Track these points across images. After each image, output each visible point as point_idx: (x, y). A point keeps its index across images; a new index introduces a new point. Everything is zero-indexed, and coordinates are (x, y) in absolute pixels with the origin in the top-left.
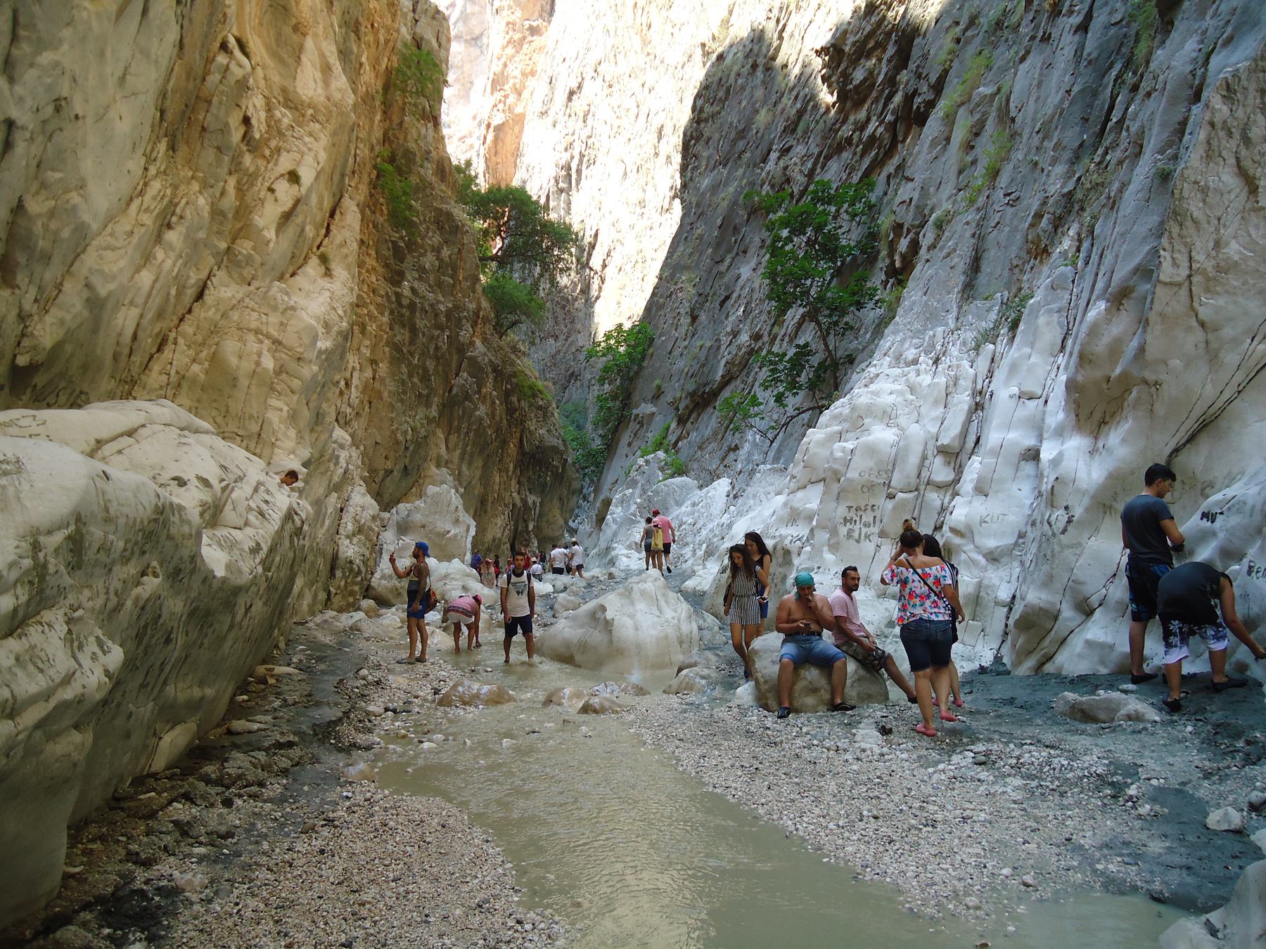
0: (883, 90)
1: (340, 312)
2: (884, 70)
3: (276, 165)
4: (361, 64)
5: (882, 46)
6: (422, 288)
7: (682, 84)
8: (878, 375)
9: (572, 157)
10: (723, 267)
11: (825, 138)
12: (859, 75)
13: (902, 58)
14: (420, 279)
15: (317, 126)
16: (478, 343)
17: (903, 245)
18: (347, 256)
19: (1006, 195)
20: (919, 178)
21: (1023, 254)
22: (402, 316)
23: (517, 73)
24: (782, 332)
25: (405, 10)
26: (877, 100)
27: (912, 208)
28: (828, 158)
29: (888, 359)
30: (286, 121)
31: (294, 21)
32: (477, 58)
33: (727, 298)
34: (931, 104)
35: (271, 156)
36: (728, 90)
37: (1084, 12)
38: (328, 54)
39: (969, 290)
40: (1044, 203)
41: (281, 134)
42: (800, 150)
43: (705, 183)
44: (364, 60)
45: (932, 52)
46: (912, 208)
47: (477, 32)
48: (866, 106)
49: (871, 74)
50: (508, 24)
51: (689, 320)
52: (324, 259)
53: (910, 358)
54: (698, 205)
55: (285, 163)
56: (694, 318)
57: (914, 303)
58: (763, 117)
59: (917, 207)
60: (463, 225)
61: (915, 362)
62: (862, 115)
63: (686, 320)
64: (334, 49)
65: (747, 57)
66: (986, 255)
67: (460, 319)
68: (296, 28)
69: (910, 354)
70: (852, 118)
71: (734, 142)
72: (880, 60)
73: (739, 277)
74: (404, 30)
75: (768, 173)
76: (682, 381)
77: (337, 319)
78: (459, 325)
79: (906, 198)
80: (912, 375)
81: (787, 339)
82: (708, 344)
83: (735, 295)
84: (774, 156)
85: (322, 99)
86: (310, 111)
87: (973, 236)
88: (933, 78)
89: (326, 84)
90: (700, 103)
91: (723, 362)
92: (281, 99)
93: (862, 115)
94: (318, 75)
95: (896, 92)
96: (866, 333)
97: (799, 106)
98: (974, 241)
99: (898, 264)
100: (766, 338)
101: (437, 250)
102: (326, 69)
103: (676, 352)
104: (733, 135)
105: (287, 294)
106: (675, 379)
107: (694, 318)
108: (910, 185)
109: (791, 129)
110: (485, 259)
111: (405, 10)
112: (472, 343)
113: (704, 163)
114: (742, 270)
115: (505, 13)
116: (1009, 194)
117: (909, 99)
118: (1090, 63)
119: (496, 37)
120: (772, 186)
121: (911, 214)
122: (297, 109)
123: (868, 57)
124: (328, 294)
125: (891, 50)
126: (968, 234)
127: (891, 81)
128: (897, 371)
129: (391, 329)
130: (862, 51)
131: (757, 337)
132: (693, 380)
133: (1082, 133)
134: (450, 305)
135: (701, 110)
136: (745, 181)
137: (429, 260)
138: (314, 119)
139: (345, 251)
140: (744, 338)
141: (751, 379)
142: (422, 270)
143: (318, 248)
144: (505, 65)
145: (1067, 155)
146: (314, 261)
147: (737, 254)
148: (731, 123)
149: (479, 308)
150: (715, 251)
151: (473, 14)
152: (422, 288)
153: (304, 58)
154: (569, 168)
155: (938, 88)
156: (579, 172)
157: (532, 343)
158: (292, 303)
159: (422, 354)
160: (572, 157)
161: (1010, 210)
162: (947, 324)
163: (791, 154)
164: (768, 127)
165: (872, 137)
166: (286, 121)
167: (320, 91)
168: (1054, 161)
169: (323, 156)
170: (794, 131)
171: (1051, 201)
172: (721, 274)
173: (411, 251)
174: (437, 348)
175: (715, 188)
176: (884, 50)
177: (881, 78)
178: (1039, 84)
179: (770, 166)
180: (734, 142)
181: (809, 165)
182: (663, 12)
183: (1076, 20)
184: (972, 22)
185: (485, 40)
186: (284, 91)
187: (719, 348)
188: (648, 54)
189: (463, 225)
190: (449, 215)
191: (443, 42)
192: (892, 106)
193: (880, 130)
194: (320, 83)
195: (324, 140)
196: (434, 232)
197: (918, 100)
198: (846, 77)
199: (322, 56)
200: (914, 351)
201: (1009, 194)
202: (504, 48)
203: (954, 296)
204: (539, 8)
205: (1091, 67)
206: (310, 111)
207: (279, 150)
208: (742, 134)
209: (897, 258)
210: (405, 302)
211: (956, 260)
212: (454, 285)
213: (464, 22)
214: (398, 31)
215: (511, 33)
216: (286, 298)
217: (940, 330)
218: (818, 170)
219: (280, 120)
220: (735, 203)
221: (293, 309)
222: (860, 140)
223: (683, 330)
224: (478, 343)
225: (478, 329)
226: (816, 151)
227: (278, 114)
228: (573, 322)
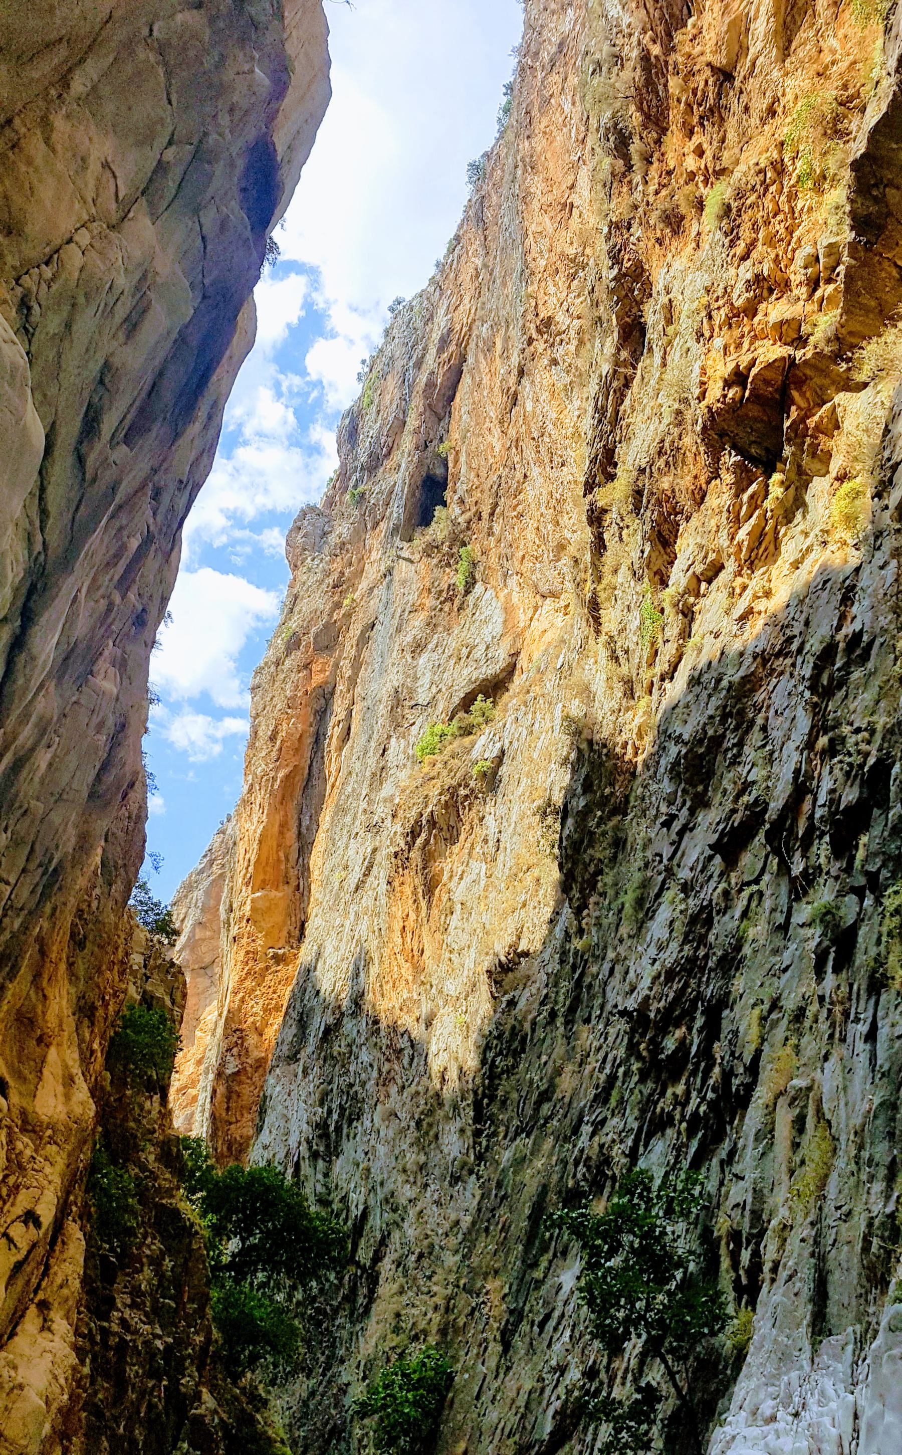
0: (697, 1065)
1: (62, 1381)
2: (696, 1041)
3: (13, 1205)
4: (93, 1052)
5: (689, 1014)
6: (134, 1318)
7: (467, 1018)
8: (734, 1438)
9: (330, 1112)
10: (538, 1274)
11: (643, 1111)
12: (670, 1044)
13: (712, 1031)
14: (133, 1306)
15: (54, 1148)
16: (206, 1396)
17: (745, 1256)
18: (67, 1300)
19: (838, 1208)
20: (751, 1176)
21: (864, 1282)
22: (108, 1361)
23: (257, 1009)
24: (625, 1365)
25: (135, 967)
26: (694, 1073)
27: (747, 1213)
28: (650, 1136)
29: (743, 1413)
30: (28, 1152)
31: (39, 1032)
32: (206, 989)
33: (548, 1317)
34: (750, 1088)
35: (9, 1196)
36: (524, 1039)
37: (869, 1021)
38: (70, 1063)
39: (820, 1326)
40: (870, 1225)
41: (21, 1167)
42: (615, 1122)
43: (506, 1156)
44: (96, 1046)
45: (741, 1029)
46: (747, 1213)
47: (207, 960)
48: (683, 1081)
49: (683, 1046)
50: (247, 953)
51: (500, 1349)
52: (44, 1306)
53: (768, 1413)
54: (499, 1185)
55: (23, 1202)
56: (507, 1346)
57: (764, 1337)
58: (566, 1083)
59: (753, 1212)
60: (192, 1225)
61: (773, 1419)
62: (680, 1089)
63: (495, 1348)
64: (76, 1056)
65: (542, 1004)
66: (830, 1278)
67: (183, 1358)
68: (40, 1040)
69: (767, 1408)
70: (670, 1092)
71: (538, 1104)
72: (690, 1029)
73: (560, 1287)
74: (132, 989)
75: (582, 1151)
76: (495, 1442)
77: (58, 1391)
78: (181, 1370)
79: (740, 1200)
80: (771, 1437)
81: (630, 1377)
82: (528, 1386)
83: (556, 1314)
84: (587, 1129)
85: (63, 1116)
86: (49, 1132)
87: (812, 1255)
88: (747, 1059)
89: (67, 1097)
90: (490, 1055)
91: (551, 1412)
92: (19, 1123)
93: (680, 1089)
94: (60, 1089)
95: (714, 1065)
96: (725, 1368)
97: (607, 1071)
98: (813, 1261)
99: (744, 1281)
100: (603, 1375)
101: (156, 1262)
102: (69, 1081)
103: (486, 1397)
104: (534, 1097)
105: (15, 1368)
106: (486, 1440)
107: (507, 1346)
108: (741, 1183)
109: (602, 1097)
110: (218, 1267)
111: (135, 967)
112: (198, 1396)
113: (502, 1129)
114: (563, 1278)
115: (244, 941)
116: (839, 1208)
117: (728, 1075)
118: (883, 1075)
119: (231, 973)
120: (589, 1168)
121: (747, 1219)
122: (34, 1131)
123: (677, 1026)
124: (48, 1357)
125: (699, 1022)
126: (806, 1253)
127: (706, 1053)
128: (755, 1431)
129: (93, 1383)
130: (670, 1019)
131: (591, 1373)
132: (510, 1442)
133: (891, 1149)
134: (170, 1340)
135: (493, 1064)
136: (555, 1158)
137: (146, 1278)
138: (52, 1140)
139: (65, 1291)
140: (574, 1375)
141: (589, 1438)
142: (136, 1291)
143: (36, 1292)
144: (242, 1000)
145: (882, 1172)
146: (33, 1310)
147: (555, 1256)
148: (531, 1081)
149: (208, 1340)
150: (527, 1250)
151: (204, 940)
152: (134, 1318)
153: (46, 1071)
154: (326, 1126)
155: (753, 1069)
156: (338, 1129)
157: (273, 1383)
158: (19, 1380)
159: (129, 1419)
160: (330, 1112)
161: (844, 1227)
162: (801, 1368)
163: (606, 1129)
164: (575, 1092)
165: (696, 1113)
166: (28, 1152)
167: (60, 1108)
168: (872, 1178)
169: (58, 1181)
170: (606, 1101)
171: (877, 1222)
172: (539, 1283)
173: (123, 1267)
174: (151, 1407)
175: (520, 1162)
176: (693, 1019)
177: (694, 1049)
178: (845, 1089)
179: (583, 1141)
180: (538, 1104)
181: (630, 1142)
182: (438, 935)
183: (863, 1028)
184: (775, 1005)
185: (217, 970)
186: (23, 1113)
187: (543, 1390)
188: (423, 983)
189: (192, 1225)
190: (176, 1213)
191: (178, 998)
192: (711, 1082)
193: (703, 1108)
194: (61, 1099)
195: (61, 1162)
196: (154, 1238)
197: (736, 1082)
198: (656, 1047)
199: (66, 1067)
200: (771, 1403)
201: (839, 1208)
202: (242, 980)
203: (804, 1330)
204: (285, 933)
205: (885, 1080)
206: (49, 1132)
207: (17, 1187)
208: (545, 1096)
209: (741, 1272)
210: (113, 1341)
211: (798, 1285)
212: (176, 1311)
213: (192, 950)
214: (125, 992)
215: (251, 963)
216: (13, 1373)
217: (794, 1374)
218: (641, 1149)
219: (21, 1153)
220: (544, 1189)
221: (21, 1387)
222: (683, 1116)
223: (492, 1362)
224: (206, 1396)
225: (206, 1373)
226: (635, 1125)
227: (19, 1146)
228: (333, 1346)
